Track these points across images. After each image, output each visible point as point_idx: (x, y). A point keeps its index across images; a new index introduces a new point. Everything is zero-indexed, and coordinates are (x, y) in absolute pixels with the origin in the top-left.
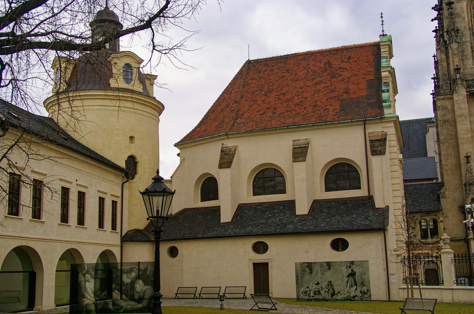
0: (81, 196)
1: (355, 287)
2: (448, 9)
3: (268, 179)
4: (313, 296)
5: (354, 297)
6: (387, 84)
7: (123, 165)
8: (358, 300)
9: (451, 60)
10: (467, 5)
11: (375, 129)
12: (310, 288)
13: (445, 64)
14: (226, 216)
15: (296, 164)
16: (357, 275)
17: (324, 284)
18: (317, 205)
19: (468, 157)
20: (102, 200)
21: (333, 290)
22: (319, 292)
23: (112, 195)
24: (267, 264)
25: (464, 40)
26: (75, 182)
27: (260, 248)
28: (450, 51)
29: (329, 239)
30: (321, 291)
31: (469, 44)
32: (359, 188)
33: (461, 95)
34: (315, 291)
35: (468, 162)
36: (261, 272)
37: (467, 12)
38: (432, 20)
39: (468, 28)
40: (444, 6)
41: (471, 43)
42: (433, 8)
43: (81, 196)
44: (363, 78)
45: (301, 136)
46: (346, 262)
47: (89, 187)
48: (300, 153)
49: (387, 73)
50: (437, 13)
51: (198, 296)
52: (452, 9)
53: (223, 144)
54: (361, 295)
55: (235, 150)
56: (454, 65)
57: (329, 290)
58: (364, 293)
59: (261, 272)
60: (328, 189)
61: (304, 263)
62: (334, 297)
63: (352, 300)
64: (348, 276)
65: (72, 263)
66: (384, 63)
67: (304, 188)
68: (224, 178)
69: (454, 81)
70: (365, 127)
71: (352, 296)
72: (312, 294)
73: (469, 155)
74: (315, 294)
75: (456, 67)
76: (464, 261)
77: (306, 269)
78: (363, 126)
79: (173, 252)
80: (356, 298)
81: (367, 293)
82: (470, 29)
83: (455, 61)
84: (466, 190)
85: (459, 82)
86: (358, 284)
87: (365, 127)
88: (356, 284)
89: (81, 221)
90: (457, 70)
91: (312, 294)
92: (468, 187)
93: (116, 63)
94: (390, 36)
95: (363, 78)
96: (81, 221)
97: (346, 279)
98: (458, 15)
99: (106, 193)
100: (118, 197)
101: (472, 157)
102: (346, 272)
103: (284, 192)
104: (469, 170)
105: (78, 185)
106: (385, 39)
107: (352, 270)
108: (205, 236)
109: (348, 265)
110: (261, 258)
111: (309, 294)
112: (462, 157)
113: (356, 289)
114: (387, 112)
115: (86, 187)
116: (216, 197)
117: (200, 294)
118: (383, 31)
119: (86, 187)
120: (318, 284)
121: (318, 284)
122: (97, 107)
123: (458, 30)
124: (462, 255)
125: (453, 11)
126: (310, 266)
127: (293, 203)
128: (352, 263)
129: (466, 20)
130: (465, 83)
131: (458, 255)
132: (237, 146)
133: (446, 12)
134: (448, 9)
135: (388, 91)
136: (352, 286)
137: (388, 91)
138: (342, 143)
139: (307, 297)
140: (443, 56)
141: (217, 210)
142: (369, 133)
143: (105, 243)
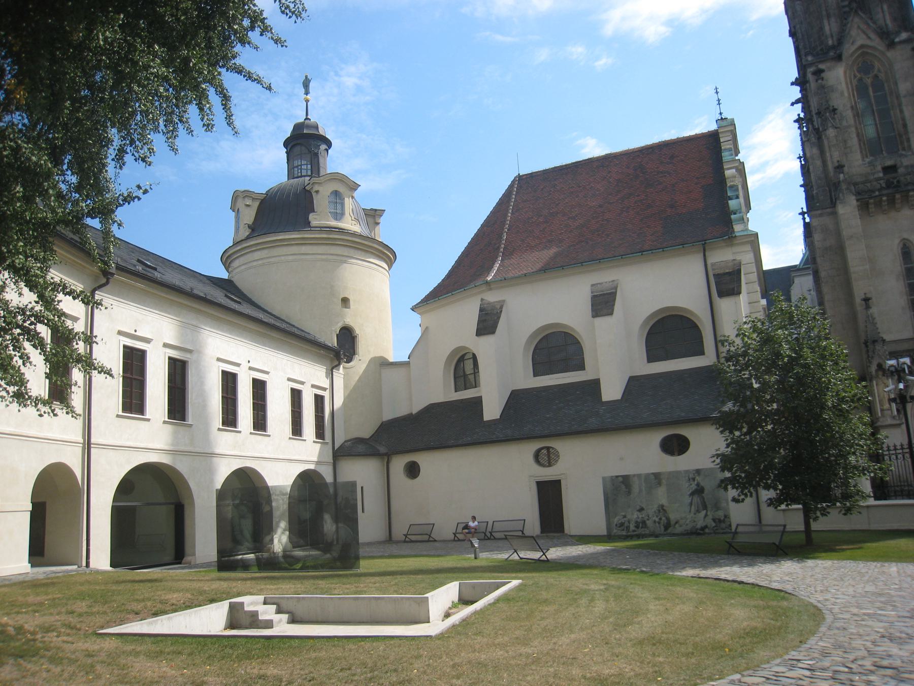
0: (259, 388)
1: (704, 512)
2: (817, 81)
3: (556, 349)
4: (634, 531)
5: (703, 529)
6: (734, 188)
7: (333, 342)
8: (709, 534)
9: (828, 154)
10: (845, 73)
11: (721, 256)
12: (629, 517)
13: (819, 163)
14: (492, 410)
15: (598, 321)
16: (706, 492)
17: (651, 510)
18: (635, 385)
19: (867, 300)
20: (296, 396)
21: (668, 519)
22: (644, 522)
23: (313, 386)
24: (559, 481)
25: (844, 123)
26: (245, 366)
27: (545, 457)
28: (826, 142)
29: (656, 437)
30: (647, 522)
31: (853, 129)
32: (702, 353)
33: (848, 209)
34: (636, 522)
35: (868, 307)
36: (550, 496)
37: (847, 83)
38: (792, 104)
39: (849, 106)
40: (810, 77)
41: (856, 128)
42: (792, 84)
43: (259, 388)
44: (696, 184)
45: (604, 277)
46: (687, 472)
47: (272, 373)
48: (603, 303)
49: (734, 170)
50: (798, 88)
51: (489, 535)
52: (822, 79)
53: (482, 300)
54: (714, 524)
55: (501, 307)
56: (833, 162)
57: (660, 519)
58: (720, 521)
59: (550, 496)
60: (651, 358)
61: (617, 477)
62: (669, 531)
63: (699, 534)
64: (692, 494)
65: (246, 488)
66: (726, 156)
67: (614, 358)
68: (486, 350)
69: (836, 185)
70: (704, 255)
71: (699, 526)
72: (632, 527)
73: (868, 296)
74: (637, 527)
75: (837, 164)
76: (900, 456)
77: (618, 489)
78: (702, 254)
79: (413, 470)
80: (707, 530)
81: (724, 521)
82: (852, 107)
83: (833, 156)
84: (868, 351)
85: (844, 186)
86: (709, 506)
87: (704, 255)
88: (705, 507)
89: (260, 424)
90: (840, 168)
91: (632, 527)
92: (871, 346)
93: (317, 192)
94: (733, 120)
95: (696, 184)
96: (260, 424)
97: (687, 500)
98: (832, 89)
99: (302, 383)
100: (324, 389)
101: (874, 299)
102: (687, 488)
103: (581, 367)
104: (871, 320)
105: (251, 368)
106: (724, 123)
107: (698, 485)
108: (460, 442)
109: (691, 476)
110: (548, 474)
111: (628, 528)
112: (858, 300)
113: (706, 515)
114: (737, 228)
115: (267, 373)
116: (476, 385)
117: (491, 533)
118: (721, 114)
119: (267, 373)
120: (641, 510)
121: (641, 510)
122: (290, 258)
123: (834, 110)
124: (895, 446)
125: (824, 83)
126: (626, 480)
127: (595, 385)
128: (698, 472)
129: (846, 94)
130: (853, 188)
131: (895, 446)
132: (504, 301)
133: (813, 85)
134: (817, 81)
135: (737, 197)
136: (698, 511)
137: (737, 197)
138: (669, 283)
139: (624, 533)
140: (815, 151)
141: (477, 403)
142: (713, 265)
143: (304, 458)
